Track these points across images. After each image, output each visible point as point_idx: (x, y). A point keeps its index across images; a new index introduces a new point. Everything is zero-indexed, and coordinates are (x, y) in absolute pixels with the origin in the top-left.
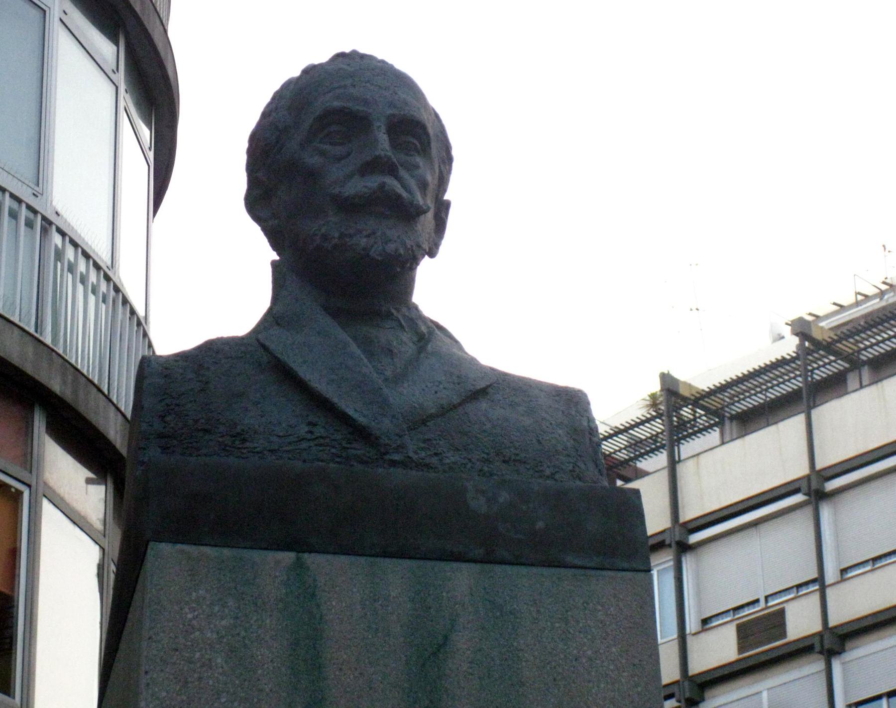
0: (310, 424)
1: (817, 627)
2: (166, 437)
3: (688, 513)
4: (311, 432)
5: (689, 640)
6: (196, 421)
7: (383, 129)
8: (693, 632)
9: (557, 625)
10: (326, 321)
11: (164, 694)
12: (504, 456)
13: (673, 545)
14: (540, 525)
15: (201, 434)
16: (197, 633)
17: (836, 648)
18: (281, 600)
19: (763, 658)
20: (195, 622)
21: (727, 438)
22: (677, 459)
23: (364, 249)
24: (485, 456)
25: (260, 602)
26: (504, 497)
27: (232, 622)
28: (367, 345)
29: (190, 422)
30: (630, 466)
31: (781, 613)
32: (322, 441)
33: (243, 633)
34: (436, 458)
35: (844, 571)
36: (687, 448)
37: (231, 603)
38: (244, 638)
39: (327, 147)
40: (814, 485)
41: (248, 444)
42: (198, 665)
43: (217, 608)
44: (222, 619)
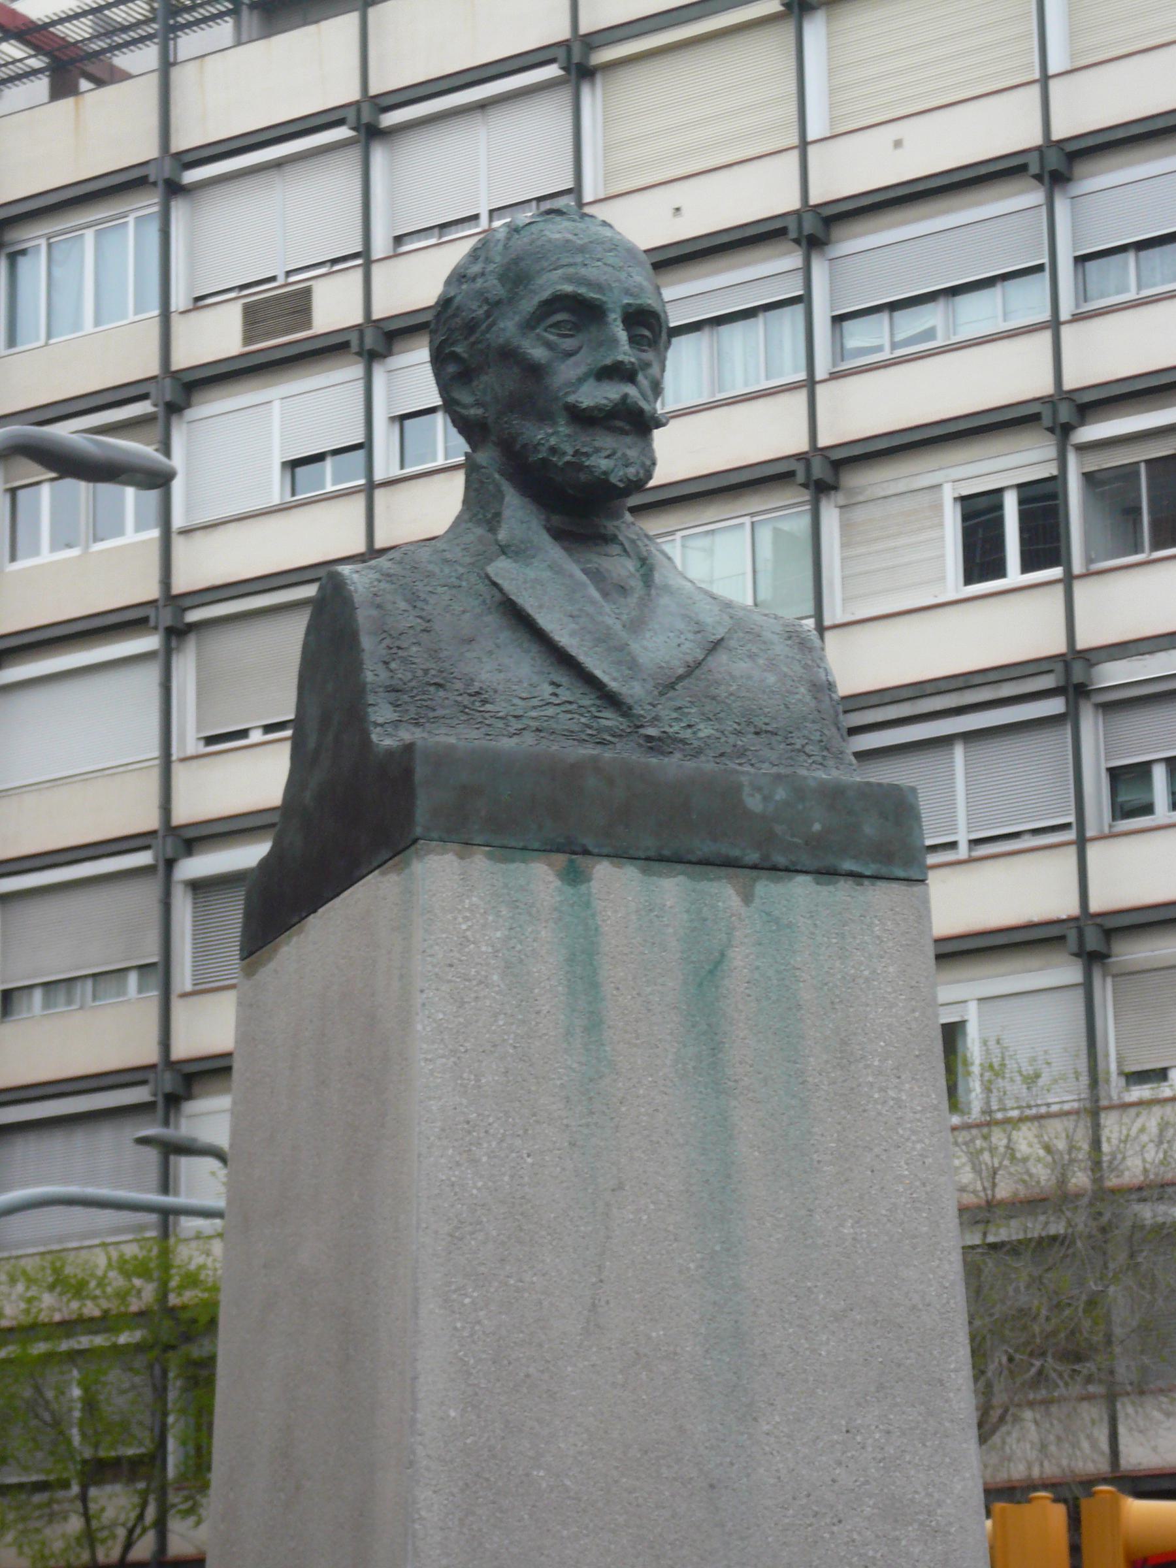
0: (553, 683)
1: (357, 318)
2: (397, 691)
3: (182, 141)
4: (555, 695)
5: (175, 320)
6: (426, 671)
7: (619, 323)
8: (181, 309)
9: (834, 941)
10: (555, 552)
11: (441, 1016)
12: (755, 726)
13: (160, 183)
14: (817, 827)
15: (432, 689)
16: (472, 946)
17: (380, 349)
18: (556, 909)
19: (278, 355)
20: (468, 933)
21: (244, 38)
22: (172, 59)
23: (605, 473)
24: (735, 726)
25: (534, 910)
26: (781, 794)
27: (507, 933)
28: (597, 576)
29: (420, 673)
30: (101, 61)
31: (307, 293)
32: (570, 707)
33: (519, 947)
34: (689, 731)
35: (399, 240)
36: (188, 44)
37: (504, 912)
38: (519, 952)
39: (552, 338)
40: (365, 119)
41: (488, 707)
42: (474, 983)
43: (491, 918)
44: (497, 929)
